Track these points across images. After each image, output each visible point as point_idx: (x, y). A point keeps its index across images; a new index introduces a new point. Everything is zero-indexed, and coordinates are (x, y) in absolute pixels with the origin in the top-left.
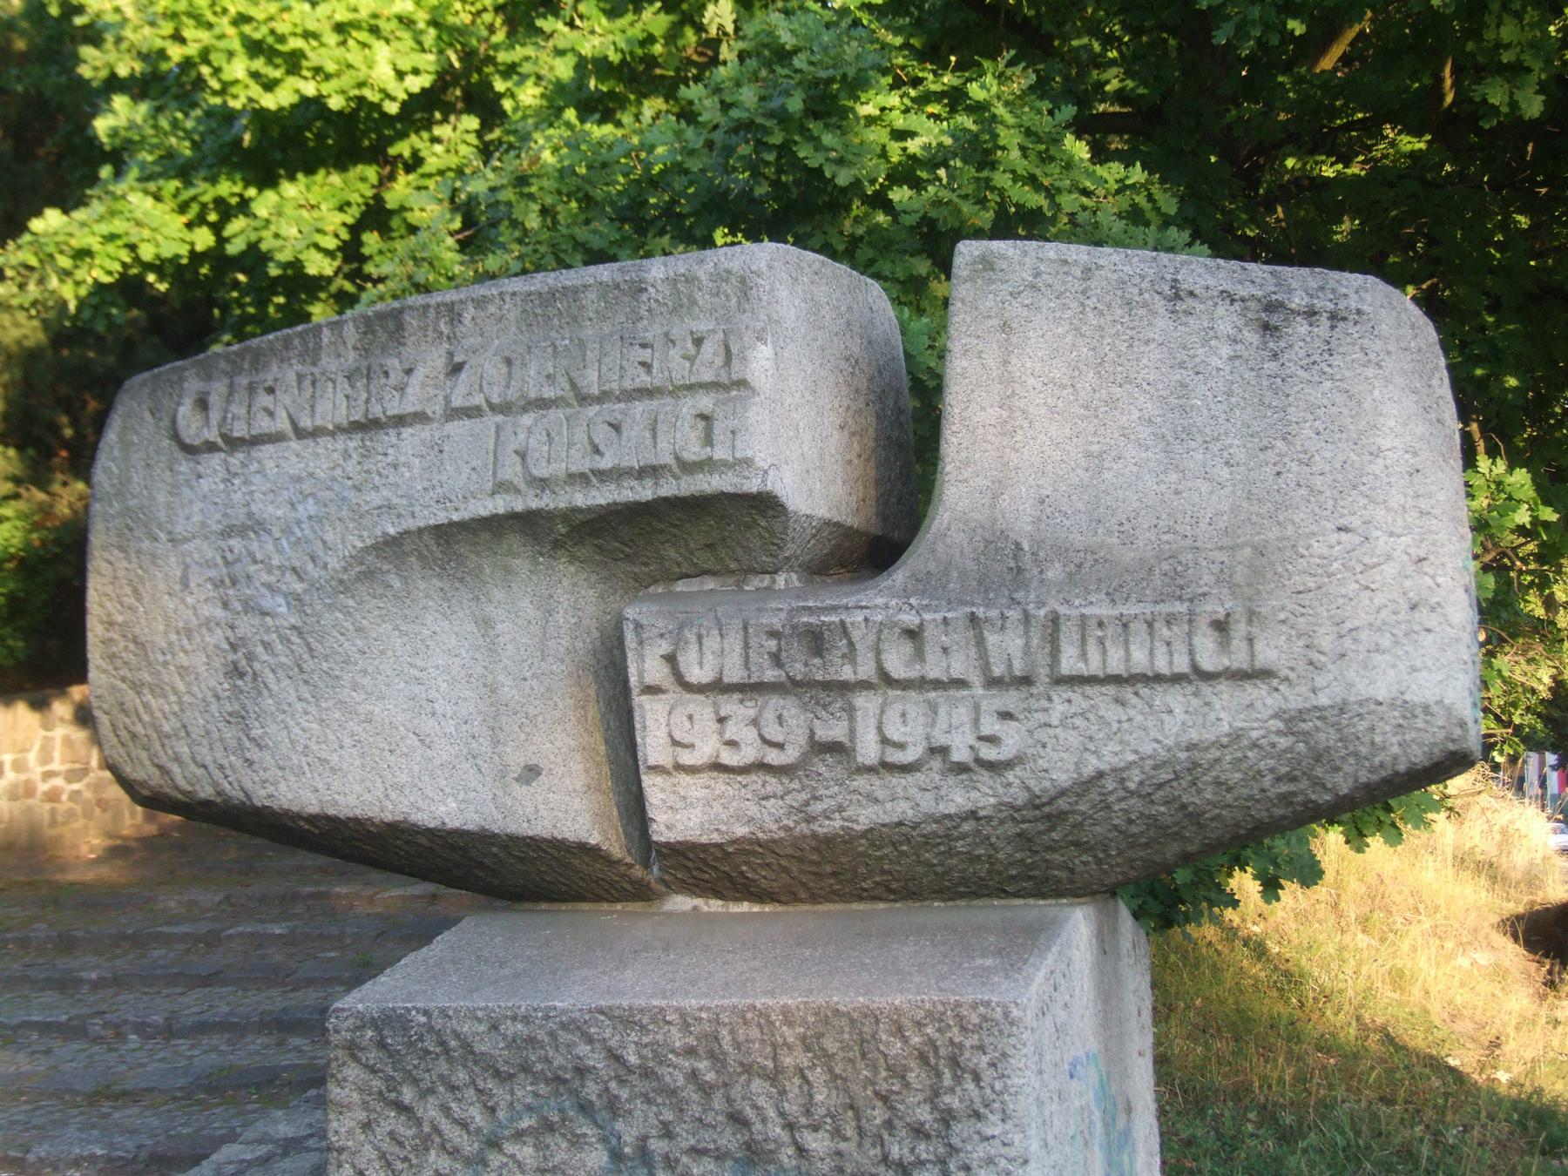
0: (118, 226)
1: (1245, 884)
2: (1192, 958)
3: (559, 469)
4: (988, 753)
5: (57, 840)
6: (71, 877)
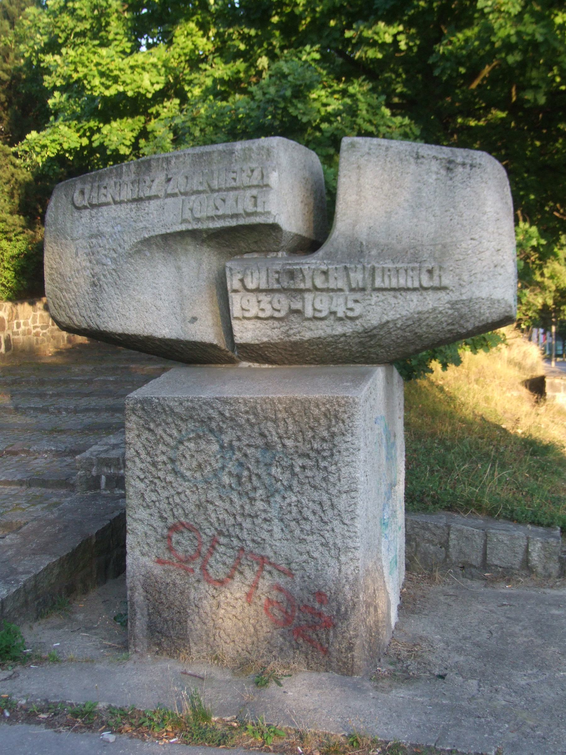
0: (56, 137)
1: (435, 365)
2: (419, 390)
3: (204, 215)
4: (350, 314)
5: (39, 349)
6: (43, 361)
